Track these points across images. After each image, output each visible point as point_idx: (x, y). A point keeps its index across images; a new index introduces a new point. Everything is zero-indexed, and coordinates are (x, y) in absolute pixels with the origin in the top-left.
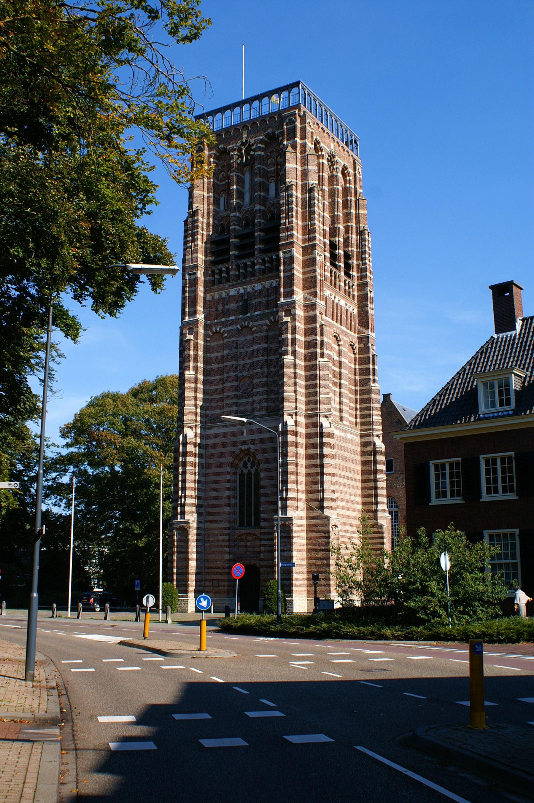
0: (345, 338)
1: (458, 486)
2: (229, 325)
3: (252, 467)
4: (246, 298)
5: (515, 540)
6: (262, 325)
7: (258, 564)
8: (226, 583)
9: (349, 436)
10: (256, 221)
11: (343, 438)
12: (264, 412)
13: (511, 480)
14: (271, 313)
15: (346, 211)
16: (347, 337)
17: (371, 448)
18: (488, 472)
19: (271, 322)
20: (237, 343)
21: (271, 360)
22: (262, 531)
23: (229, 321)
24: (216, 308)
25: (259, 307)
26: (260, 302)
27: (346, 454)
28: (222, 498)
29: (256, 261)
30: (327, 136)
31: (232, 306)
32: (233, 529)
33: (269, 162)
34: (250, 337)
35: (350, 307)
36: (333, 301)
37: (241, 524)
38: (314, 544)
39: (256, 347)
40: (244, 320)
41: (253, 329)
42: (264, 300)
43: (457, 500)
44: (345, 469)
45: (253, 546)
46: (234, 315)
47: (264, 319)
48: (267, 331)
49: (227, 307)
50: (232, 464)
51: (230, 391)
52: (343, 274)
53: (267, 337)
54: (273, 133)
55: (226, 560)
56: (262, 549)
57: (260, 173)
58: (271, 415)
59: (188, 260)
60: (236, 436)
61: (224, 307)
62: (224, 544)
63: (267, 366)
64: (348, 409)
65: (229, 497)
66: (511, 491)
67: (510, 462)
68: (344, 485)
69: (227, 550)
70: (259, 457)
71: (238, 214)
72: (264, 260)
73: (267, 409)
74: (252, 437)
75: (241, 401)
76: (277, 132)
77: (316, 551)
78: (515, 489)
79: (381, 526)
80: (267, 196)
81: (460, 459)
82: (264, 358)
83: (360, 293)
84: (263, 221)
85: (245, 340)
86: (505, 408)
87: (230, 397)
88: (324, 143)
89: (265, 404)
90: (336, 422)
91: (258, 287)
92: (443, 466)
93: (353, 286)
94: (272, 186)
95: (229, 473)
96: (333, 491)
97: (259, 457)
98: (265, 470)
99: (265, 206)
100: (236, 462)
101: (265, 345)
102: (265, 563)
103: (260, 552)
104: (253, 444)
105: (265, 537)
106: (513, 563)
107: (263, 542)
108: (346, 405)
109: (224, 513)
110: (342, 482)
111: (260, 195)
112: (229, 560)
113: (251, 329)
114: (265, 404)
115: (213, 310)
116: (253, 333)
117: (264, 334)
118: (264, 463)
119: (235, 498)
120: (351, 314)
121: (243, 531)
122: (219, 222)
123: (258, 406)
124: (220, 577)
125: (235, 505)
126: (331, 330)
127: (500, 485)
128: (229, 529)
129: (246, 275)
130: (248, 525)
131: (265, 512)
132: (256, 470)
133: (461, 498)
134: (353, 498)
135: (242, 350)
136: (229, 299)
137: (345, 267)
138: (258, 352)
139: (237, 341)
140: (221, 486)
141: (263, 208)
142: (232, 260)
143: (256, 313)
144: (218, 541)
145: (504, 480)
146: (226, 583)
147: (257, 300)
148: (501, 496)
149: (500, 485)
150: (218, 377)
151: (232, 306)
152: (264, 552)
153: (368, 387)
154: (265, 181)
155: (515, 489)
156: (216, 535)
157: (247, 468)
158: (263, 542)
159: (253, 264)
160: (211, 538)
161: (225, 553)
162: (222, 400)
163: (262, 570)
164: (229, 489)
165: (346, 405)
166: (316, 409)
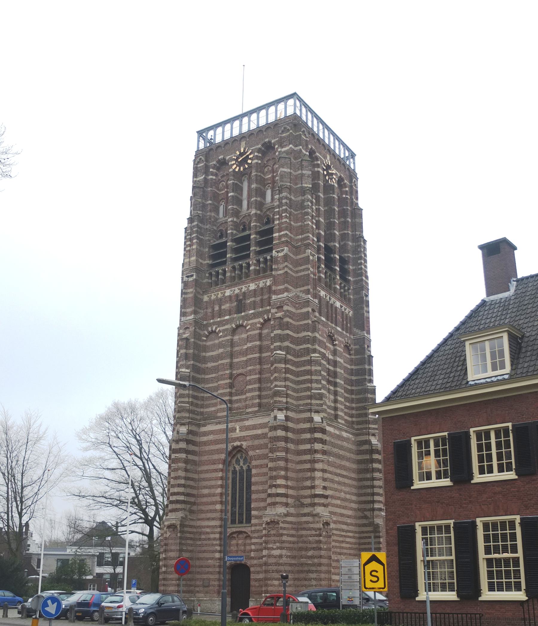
0: (340, 339)
3: (244, 464)
4: (241, 297)
5: (498, 464)
6: (256, 324)
7: (249, 563)
8: (216, 583)
9: (345, 434)
10: (252, 224)
11: (338, 436)
12: (256, 409)
16: (342, 338)
17: (366, 447)
18: (480, 448)
23: (224, 320)
25: (254, 305)
27: (341, 452)
29: (251, 263)
30: (323, 147)
31: (226, 306)
33: (266, 170)
34: (244, 336)
35: (345, 309)
36: (328, 302)
37: (233, 522)
39: (249, 345)
40: (239, 319)
41: (247, 328)
43: (446, 482)
45: (245, 545)
47: (258, 317)
49: (223, 307)
51: (224, 388)
52: (338, 277)
53: (260, 334)
54: (270, 142)
55: (216, 559)
56: (253, 547)
57: (256, 180)
61: (220, 307)
62: (215, 542)
64: (343, 407)
66: (509, 469)
67: (507, 435)
68: (339, 483)
70: (251, 453)
71: (235, 219)
72: (258, 261)
76: (273, 141)
78: (514, 467)
79: (377, 526)
80: (263, 201)
81: (446, 434)
84: (258, 224)
85: (239, 339)
88: (320, 153)
90: (330, 420)
91: (252, 286)
92: (427, 441)
93: (349, 289)
97: (251, 453)
98: (256, 467)
99: (261, 211)
102: (255, 562)
103: (251, 551)
104: (246, 441)
107: (254, 541)
109: (215, 511)
110: (337, 480)
115: (210, 310)
116: (247, 331)
118: (255, 460)
120: (347, 316)
124: (211, 577)
126: (326, 330)
129: (242, 275)
131: (257, 509)
132: (248, 466)
133: (449, 479)
134: (348, 496)
137: (340, 271)
140: (213, 483)
141: (259, 212)
142: (228, 263)
143: (251, 312)
144: (209, 539)
146: (216, 583)
148: (496, 476)
154: (262, 188)
155: (514, 467)
156: (208, 533)
157: (239, 465)
158: (254, 541)
159: (249, 265)
160: (203, 537)
161: (216, 551)
163: (252, 569)
165: (341, 403)
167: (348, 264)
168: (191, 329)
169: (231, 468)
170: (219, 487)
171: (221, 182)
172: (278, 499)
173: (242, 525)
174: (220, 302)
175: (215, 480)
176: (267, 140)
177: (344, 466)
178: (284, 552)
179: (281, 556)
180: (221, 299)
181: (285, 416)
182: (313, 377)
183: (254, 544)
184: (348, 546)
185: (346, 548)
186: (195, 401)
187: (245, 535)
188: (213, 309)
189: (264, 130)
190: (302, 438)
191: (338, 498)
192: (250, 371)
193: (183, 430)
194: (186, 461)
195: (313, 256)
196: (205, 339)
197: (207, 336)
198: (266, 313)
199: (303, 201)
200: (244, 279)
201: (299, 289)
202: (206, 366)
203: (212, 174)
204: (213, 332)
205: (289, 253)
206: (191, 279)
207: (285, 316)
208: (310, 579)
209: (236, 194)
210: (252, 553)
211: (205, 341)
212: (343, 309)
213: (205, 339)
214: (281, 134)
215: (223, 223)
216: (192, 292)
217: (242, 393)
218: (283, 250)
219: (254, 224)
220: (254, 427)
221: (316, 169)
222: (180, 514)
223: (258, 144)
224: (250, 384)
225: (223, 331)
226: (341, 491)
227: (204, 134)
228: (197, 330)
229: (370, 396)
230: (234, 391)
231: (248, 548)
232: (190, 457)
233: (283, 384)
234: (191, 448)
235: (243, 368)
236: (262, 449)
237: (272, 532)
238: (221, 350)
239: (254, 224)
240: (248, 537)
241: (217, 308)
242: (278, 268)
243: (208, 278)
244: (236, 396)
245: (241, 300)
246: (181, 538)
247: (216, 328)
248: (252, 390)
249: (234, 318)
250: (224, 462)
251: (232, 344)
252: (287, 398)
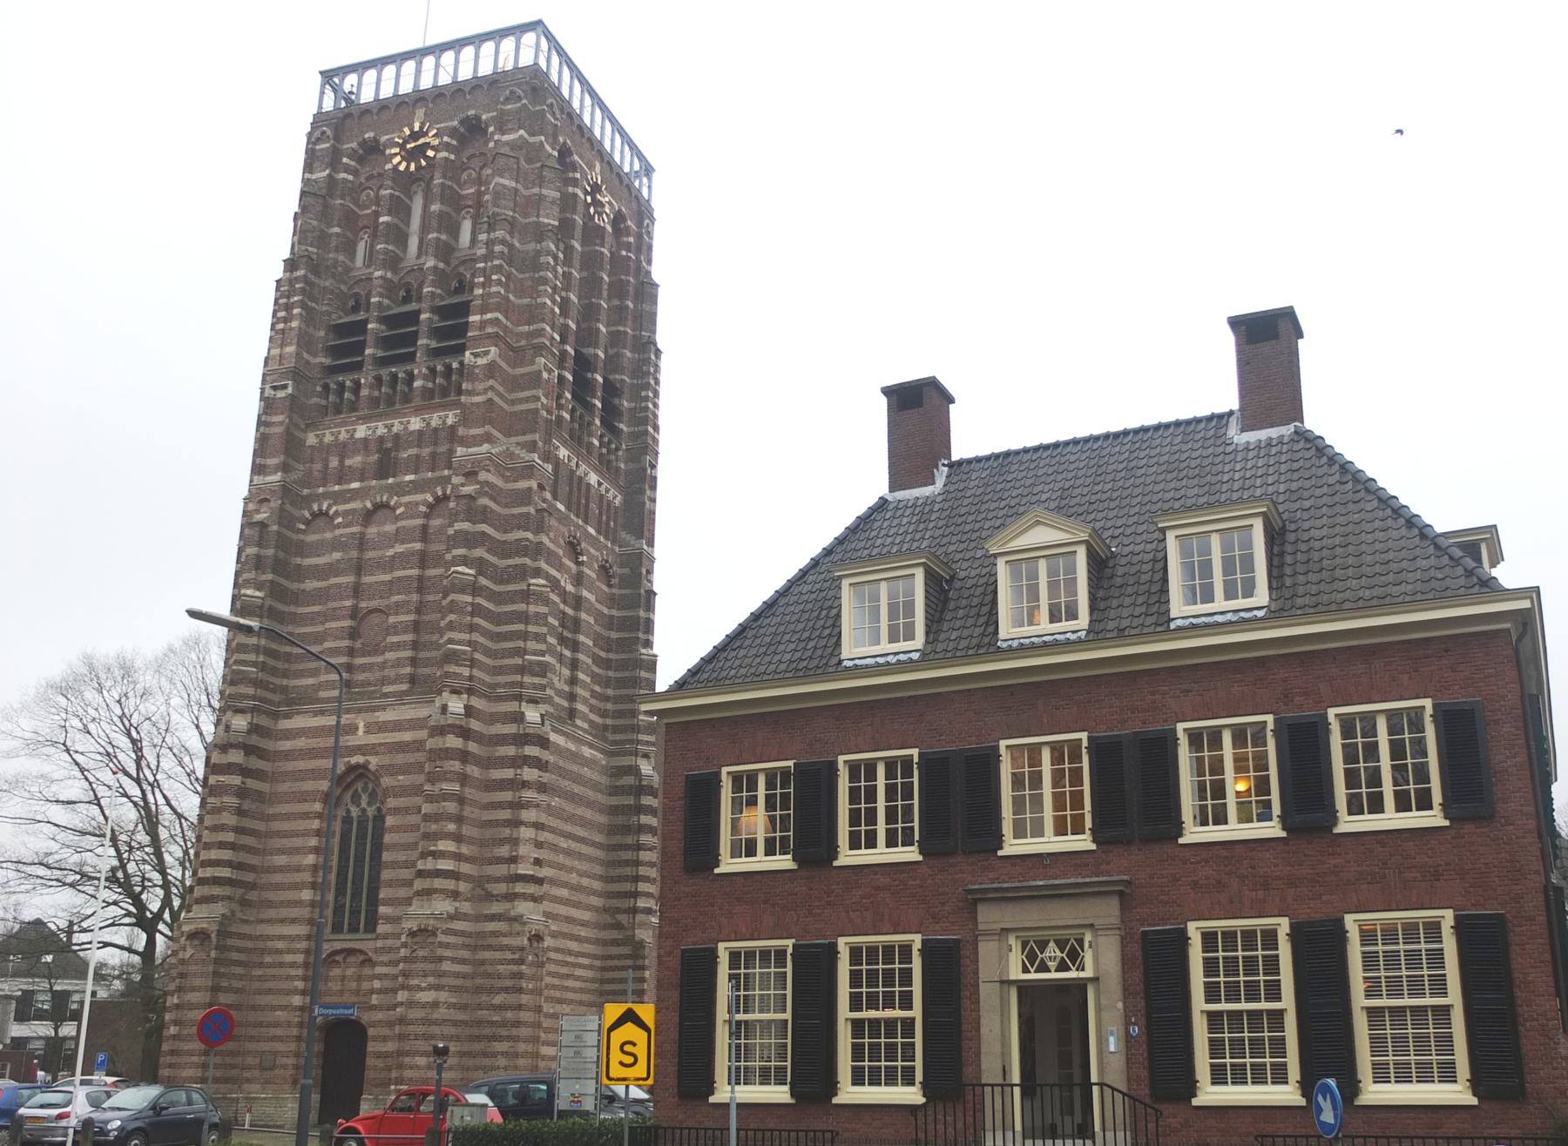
1: (785, 806)
3: (369, 804)
6: (417, 504)
7: (366, 1018)
8: (291, 1061)
9: (587, 752)
12: (404, 687)
13: (908, 816)
14: (438, 479)
15: (616, 302)
17: (629, 780)
18: (854, 795)
22: (380, 944)
25: (416, 465)
28: (298, 869)
33: (464, 176)
34: (390, 528)
35: (607, 491)
39: (400, 548)
40: (382, 490)
41: (398, 512)
43: (783, 862)
44: (571, 819)
51: (336, 638)
52: (598, 422)
53: (425, 528)
56: (377, 984)
57: (442, 196)
61: (342, 461)
62: (293, 972)
64: (587, 694)
66: (908, 842)
67: (908, 772)
68: (568, 853)
70: (386, 781)
71: (389, 275)
72: (433, 370)
74: (374, 739)
78: (917, 837)
80: (452, 242)
81: (790, 763)
83: (631, 466)
86: (903, 645)
89: (408, 670)
91: (416, 424)
92: (752, 778)
93: (617, 449)
94: (467, 226)
96: (538, 862)
97: (386, 781)
98: (396, 811)
99: (447, 263)
102: (380, 1016)
103: (372, 991)
104: (376, 754)
106: (1270, 1012)
107: (379, 970)
108: (585, 686)
115: (318, 466)
116: (398, 518)
117: (419, 521)
124: (280, 1047)
126: (565, 530)
127: (881, 828)
129: (395, 398)
132: (379, 809)
134: (585, 881)
142: (368, 366)
143: (408, 478)
144: (281, 965)
145: (891, 816)
146: (291, 1061)
148: (882, 854)
149: (881, 828)
152: (379, 992)
153: (631, 656)
155: (917, 837)
156: (278, 952)
157: (358, 805)
158: (379, 970)
160: (268, 959)
161: (295, 992)
163: (371, 1032)
165: (585, 686)
167: (620, 397)
168: (272, 504)
169: (341, 813)
172: (438, 883)
173: (357, 936)
176: (472, 112)
177: (581, 818)
178: (443, 996)
179: (435, 1005)
180: (344, 445)
181: (466, 707)
182: (531, 628)
184: (577, 984)
185: (574, 990)
186: (271, 662)
187: (362, 958)
189: (467, 89)
191: (565, 885)
193: (240, 722)
194: (242, 793)
195: (550, 371)
196: (302, 527)
197: (307, 523)
199: (538, 253)
201: (514, 439)
202: (302, 586)
203: (347, 169)
204: (322, 514)
205: (499, 361)
206: (281, 394)
207: (481, 493)
208: (494, 1055)
211: (304, 532)
212: (603, 489)
213: (302, 527)
216: (281, 423)
217: (377, 650)
218: (486, 353)
220: (397, 726)
221: (570, 189)
222: (219, 909)
224: (396, 633)
226: (571, 870)
227: (336, 80)
228: (288, 507)
229: (643, 674)
230: (358, 645)
231: (365, 985)
232: (252, 784)
233: (466, 637)
234: (255, 763)
237: (421, 953)
238: (337, 555)
240: (368, 962)
241: (334, 463)
243: (319, 395)
245: (388, 451)
246: (217, 961)
248: (397, 646)
250: (326, 798)
251: (362, 543)
252: (471, 667)
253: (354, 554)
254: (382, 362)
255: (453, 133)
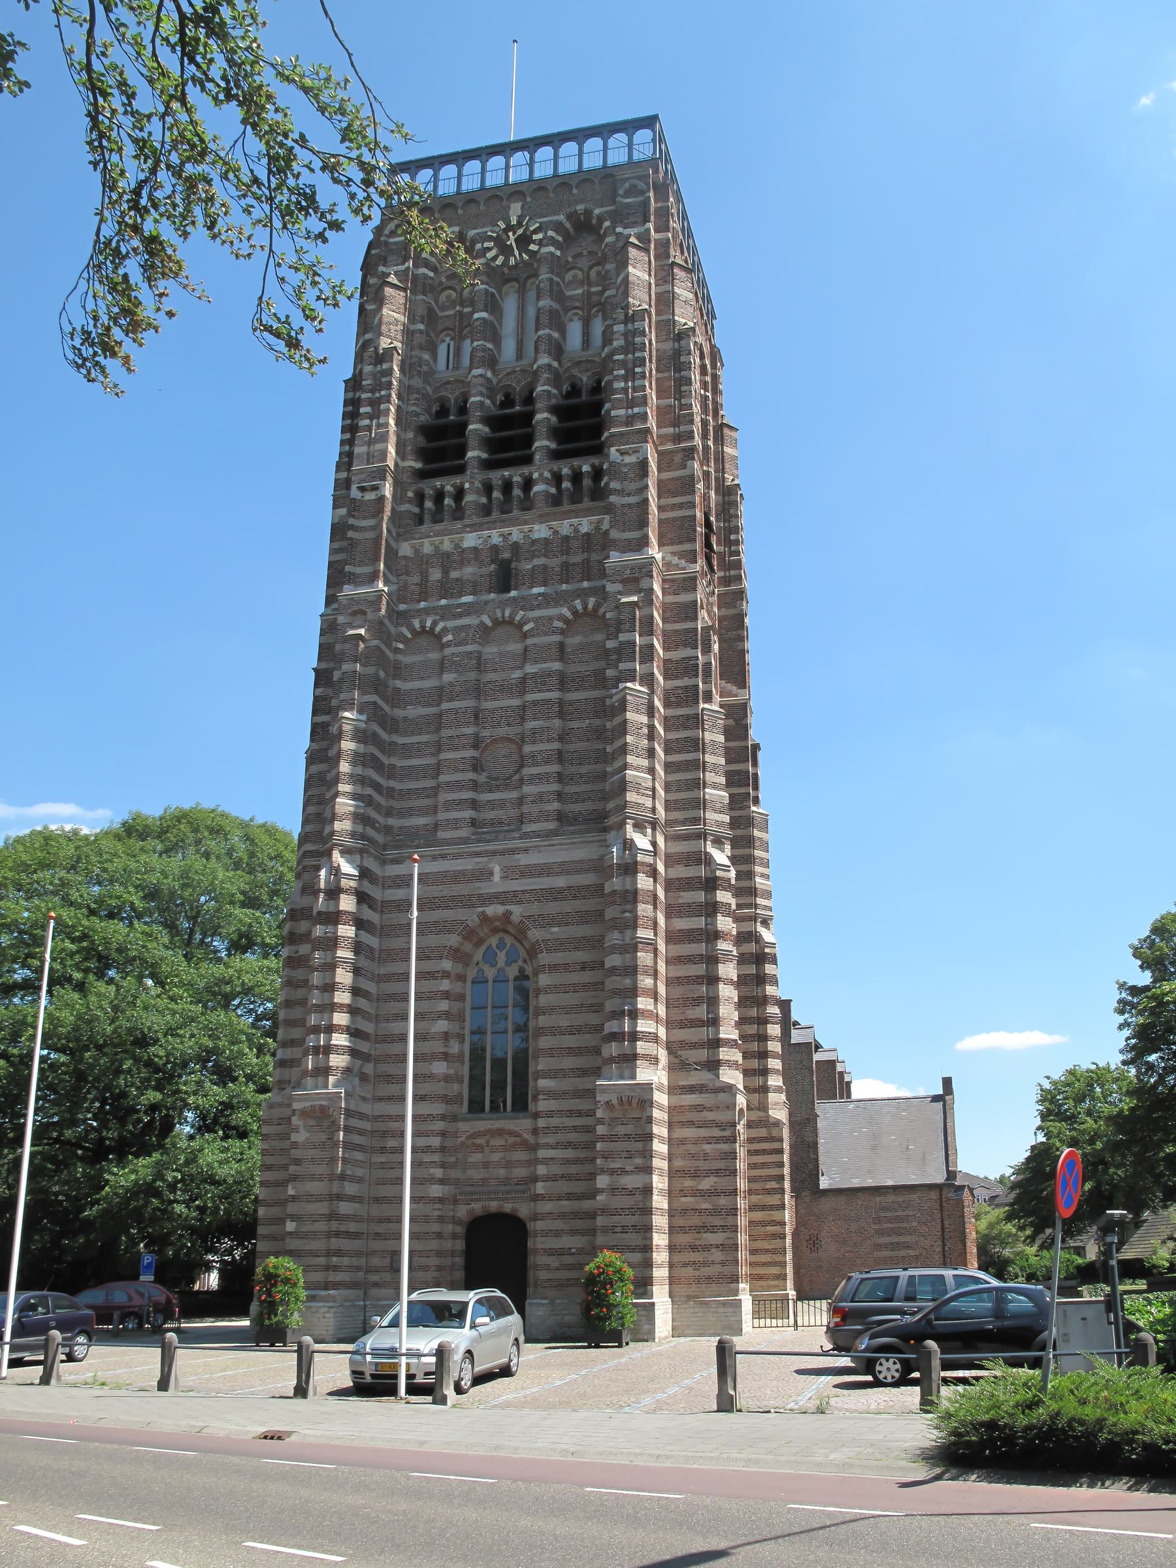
2: (460, 615)
3: (508, 963)
6: (550, 619)
7: (524, 1210)
10: (539, 389)
12: (551, 825)
14: (574, 591)
19: (575, 613)
20: (479, 659)
21: (571, 703)
24: (425, 576)
25: (542, 576)
26: (545, 567)
31: (469, 571)
32: (454, 1118)
37: (476, 1106)
38: (693, 1156)
40: (503, 605)
41: (526, 628)
42: (555, 562)
46: (474, 593)
48: (562, 632)
49: (454, 574)
50: (456, 951)
51: (456, 770)
53: (561, 646)
54: (588, 213)
57: (551, 290)
58: (573, 833)
59: (360, 455)
60: (470, 881)
61: (446, 572)
63: (561, 715)
65: (446, 1036)
69: (438, 1173)
70: (535, 934)
71: (489, 374)
73: (561, 817)
75: (485, 797)
76: (597, 212)
77: (696, 1175)
82: (554, 695)
83: (725, 612)
87: (458, 786)
89: (556, 805)
91: (541, 531)
95: (446, 975)
97: (535, 934)
100: (468, 947)
101: (557, 666)
104: (520, 902)
105: (550, 1139)
111: (550, 336)
112: (441, 1200)
113: (521, 625)
114: (556, 805)
115: (416, 579)
116: (525, 636)
117: (557, 638)
119: (461, 1038)
121: (482, 1125)
122: (436, 390)
123: (535, 809)
125: (460, 1058)
128: (443, 1117)
129: (508, 502)
130: (495, 1108)
135: (491, 676)
136: (464, 556)
138: (541, 680)
139: (480, 653)
143: (535, 590)
147: (536, 562)
150: (424, 738)
151: (469, 571)
159: (528, 484)
162: (436, 790)
164: (447, 1015)
166: (696, 820)
170: (439, 1017)
171: (443, 290)
174: (446, 561)
175: (430, 998)
183: (546, 1161)
188: (427, 577)
190: (681, 901)
192: (534, 732)
196: (401, 646)
198: (578, 596)
200: (515, 513)
208: (707, 1248)
209: (492, 318)
210: (540, 1185)
214: (621, 196)
215: (449, 383)
219: (546, 388)
223: (556, 213)
225: (457, 630)
235: (509, 725)
236: (567, 924)
239: (546, 388)
241: (436, 575)
242: (623, 490)
244: (490, 791)
247: (435, 623)
248: (540, 778)
249: (486, 603)
253: (473, 675)
254: (488, 465)
255: (558, 228)
